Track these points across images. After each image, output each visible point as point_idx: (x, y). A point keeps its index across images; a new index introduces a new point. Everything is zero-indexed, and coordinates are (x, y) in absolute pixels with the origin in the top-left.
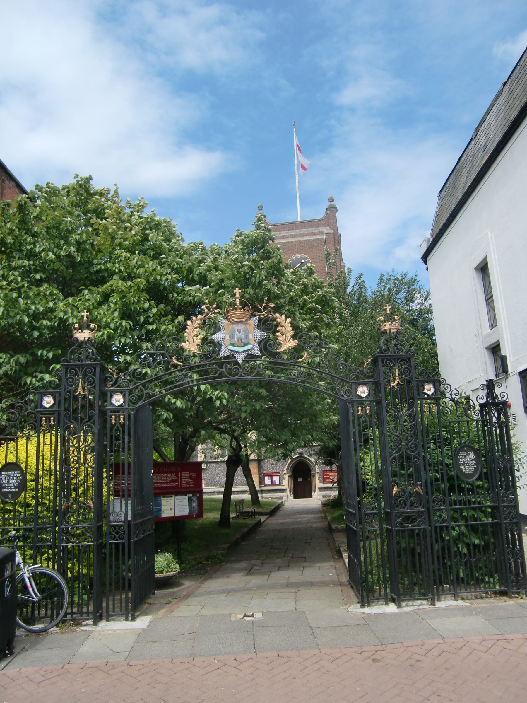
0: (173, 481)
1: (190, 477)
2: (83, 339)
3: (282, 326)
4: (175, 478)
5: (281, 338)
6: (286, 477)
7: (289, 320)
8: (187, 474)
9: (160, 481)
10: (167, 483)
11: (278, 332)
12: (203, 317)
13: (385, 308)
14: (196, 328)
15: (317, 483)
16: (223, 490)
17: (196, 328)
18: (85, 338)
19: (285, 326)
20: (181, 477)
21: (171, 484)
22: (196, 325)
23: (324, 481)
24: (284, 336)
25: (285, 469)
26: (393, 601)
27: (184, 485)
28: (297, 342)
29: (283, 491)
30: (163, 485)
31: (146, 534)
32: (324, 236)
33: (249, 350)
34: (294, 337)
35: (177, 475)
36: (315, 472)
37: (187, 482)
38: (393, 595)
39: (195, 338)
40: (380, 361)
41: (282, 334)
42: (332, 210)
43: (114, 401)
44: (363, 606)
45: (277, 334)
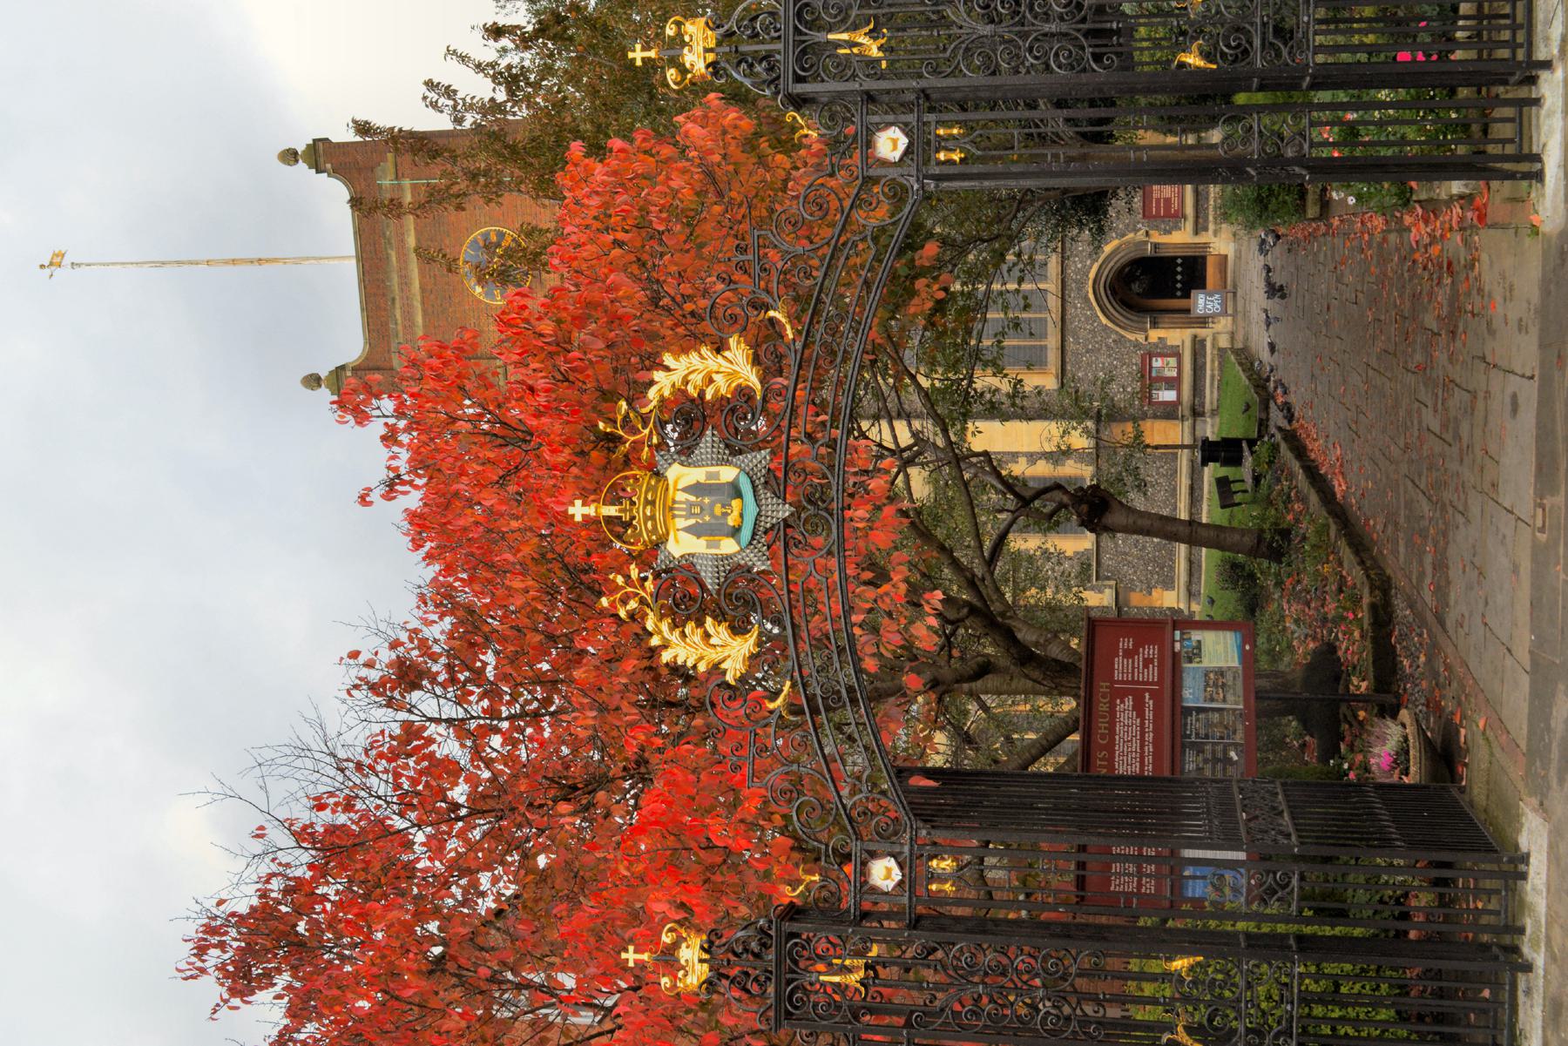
0: (1139, 708)
1: (1129, 654)
2: (706, 966)
3: (686, 382)
4: (1129, 702)
5: (722, 386)
6: (1154, 335)
7: (668, 359)
8: (1119, 663)
9: (1136, 745)
10: (1142, 724)
11: (702, 394)
12: (651, 615)
13: (631, 964)
14: (683, 635)
15: (1181, 238)
16: (1182, 549)
17: (683, 635)
18: (701, 961)
19: (685, 371)
20: (1127, 682)
21: (1149, 714)
22: (674, 637)
23: (1176, 216)
24: (715, 377)
25: (1131, 336)
26: (1532, 81)
27: (1152, 674)
28: (736, 337)
29: (1198, 346)
30: (1149, 737)
31: (1283, 807)
32: (407, 182)
33: (753, 482)
34: (720, 348)
35: (1122, 694)
36: (1146, 243)
37: (1146, 666)
38: (1513, 79)
39: (712, 641)
40: (800, 88)
41: (711, 381)
42: (321, 155)
43: (888, 885)
44: (1539, 176)
45: (708, 397)
